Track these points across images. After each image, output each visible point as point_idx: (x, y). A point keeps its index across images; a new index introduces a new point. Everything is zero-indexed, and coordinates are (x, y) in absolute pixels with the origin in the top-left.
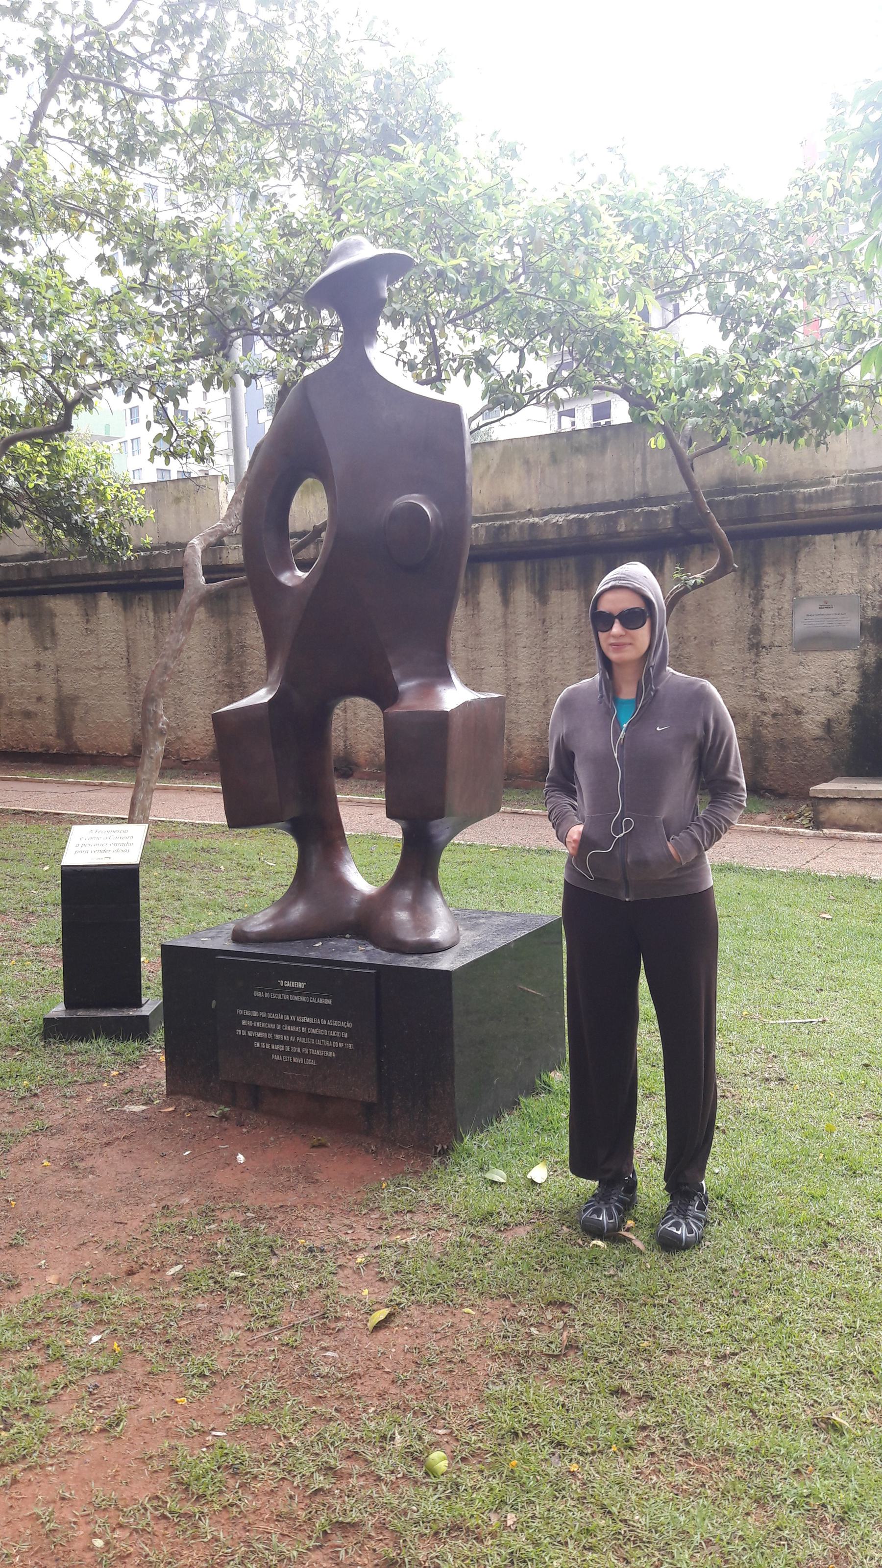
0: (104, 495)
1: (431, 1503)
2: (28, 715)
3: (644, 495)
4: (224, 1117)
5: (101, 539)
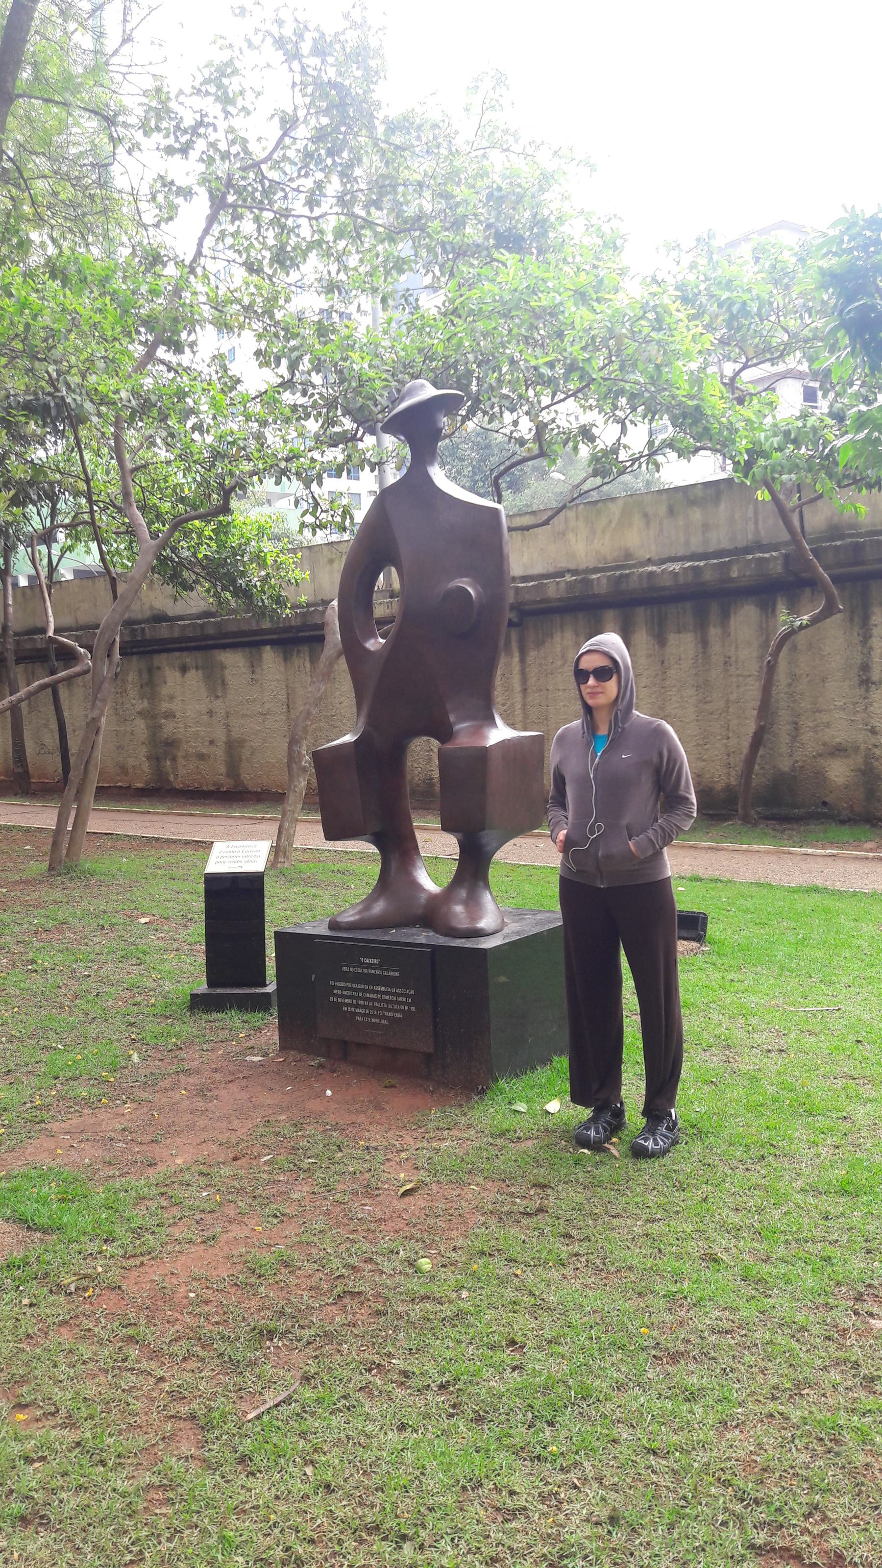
0: (265, 560)
1: (415, 1285)
2: (202, 757)
3: (757, 542)
4: (321, 1066)
5: (262, 600)
